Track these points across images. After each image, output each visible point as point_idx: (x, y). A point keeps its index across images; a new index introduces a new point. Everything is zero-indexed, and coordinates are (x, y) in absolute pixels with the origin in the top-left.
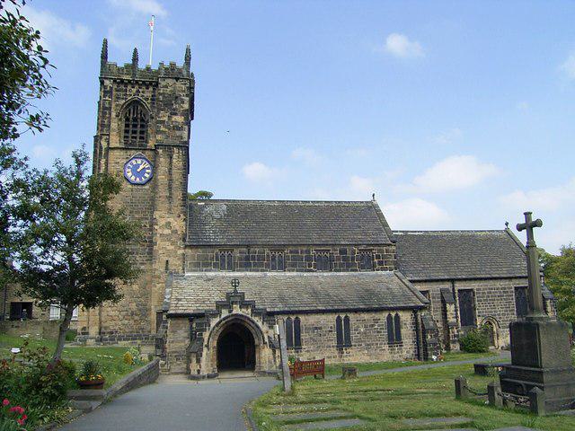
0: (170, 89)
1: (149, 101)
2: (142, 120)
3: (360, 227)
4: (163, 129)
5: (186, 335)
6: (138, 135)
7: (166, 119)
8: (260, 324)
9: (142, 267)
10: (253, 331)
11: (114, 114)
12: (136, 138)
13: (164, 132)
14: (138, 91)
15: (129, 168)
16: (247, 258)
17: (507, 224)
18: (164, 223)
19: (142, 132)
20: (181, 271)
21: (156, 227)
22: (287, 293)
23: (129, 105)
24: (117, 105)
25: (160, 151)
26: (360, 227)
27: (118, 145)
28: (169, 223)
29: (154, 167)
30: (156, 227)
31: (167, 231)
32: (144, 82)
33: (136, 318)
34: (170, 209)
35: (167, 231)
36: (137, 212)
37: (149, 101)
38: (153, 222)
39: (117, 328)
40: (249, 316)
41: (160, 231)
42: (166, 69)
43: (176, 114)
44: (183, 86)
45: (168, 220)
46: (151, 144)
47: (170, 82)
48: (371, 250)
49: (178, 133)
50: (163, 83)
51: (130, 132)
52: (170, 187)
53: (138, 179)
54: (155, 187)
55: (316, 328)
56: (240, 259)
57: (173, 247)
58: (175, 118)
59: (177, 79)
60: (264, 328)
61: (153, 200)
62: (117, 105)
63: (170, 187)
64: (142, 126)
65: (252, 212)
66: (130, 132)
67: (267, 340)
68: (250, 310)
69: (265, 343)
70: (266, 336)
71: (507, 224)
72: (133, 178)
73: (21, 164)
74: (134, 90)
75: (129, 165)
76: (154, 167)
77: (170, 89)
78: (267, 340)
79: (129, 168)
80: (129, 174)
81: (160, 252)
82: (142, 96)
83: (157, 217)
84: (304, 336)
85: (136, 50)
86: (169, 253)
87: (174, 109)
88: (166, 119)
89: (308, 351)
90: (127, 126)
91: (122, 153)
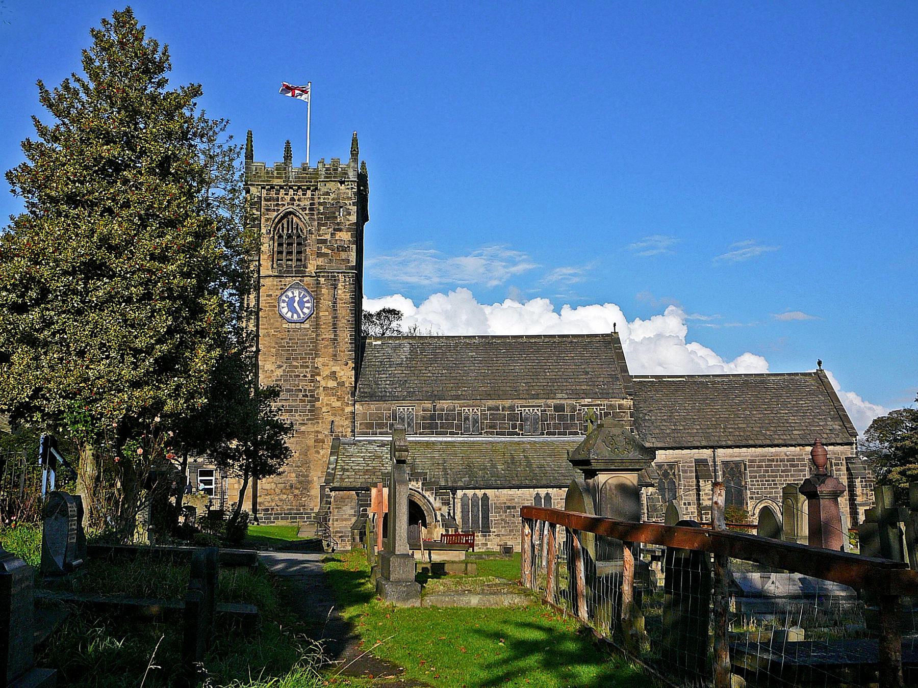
0: (332, 196)
1: (307, 212)
2: (299, 236)
3: (587, 373)
4: (324, 250)
5: (352, 512)
6: (294, 257)
7: (328, 237)
8: (432, 499)
9: (303, 428)
10: (424, 508)
11: (263, 231)
12: (291, 260)
13: (326, 255)
14: (293, 199)
15: (284, 301)
16: (432, 417)
17: (820, 363)
18: (327, 373)
19: (299, 253)
20: (349, 434)
21: (318, 378)
22: (478, 461)
23: (282, 218)
24: (267, 220)
25: (322, 280)
26: (587, 373)
27: (270, 273)
28: (335, 372)
29: (317, 300)
30: (318, 378)
31: (332, 384)
32: (299, 187)
33: (296, 492)
34: (335, 355)
35: (332, 384)
36: (296, 359)
37: (307, 212)
38: (316, 372)
39: (273, 504)
40: (420, 490)
41: (323, 383)
42: (327, 169)
43: (340, 230)
44: (350, 191)
45: (334, 369)
46: (311, 268)
47: (332, 186)
48: (598, 405)
49: (343, 255)
50: (323, 189)
51: (284, 254)
52: (335, 326)
53: (295, 316)
54: (317, 326)
55: (509, 508)
56: (424, 418)
57: (338, 404)
58: (339, 235)
59: (342, 183)
60: (437, 504)
61: (315, 342)
62: (267, 220)
63: (335, 326)
64: (299, 244)
65: (443, 354)
66: (284, 254)
67: (439, 518)
68: (420, 483)
69: (437, 521)
70: (438, 513)
71: (820, 363)
72: (289, 315)
73: (289, 429)
74: (288, 198)
75: (284, 298)
76: (317, 300)
77: (332, 196)
78: (439, 518)
79: (284, 301)
80: (285, 311)
81: (324, 409)
82: (298, 205)
83: (320, 365)
84: (492, 516)
85: (288, 142)
86: (334, 411)
87: (338, 224)
88: (328, 237)
89: (498, 535)
90: (280, 245)
91: (276, 281)
